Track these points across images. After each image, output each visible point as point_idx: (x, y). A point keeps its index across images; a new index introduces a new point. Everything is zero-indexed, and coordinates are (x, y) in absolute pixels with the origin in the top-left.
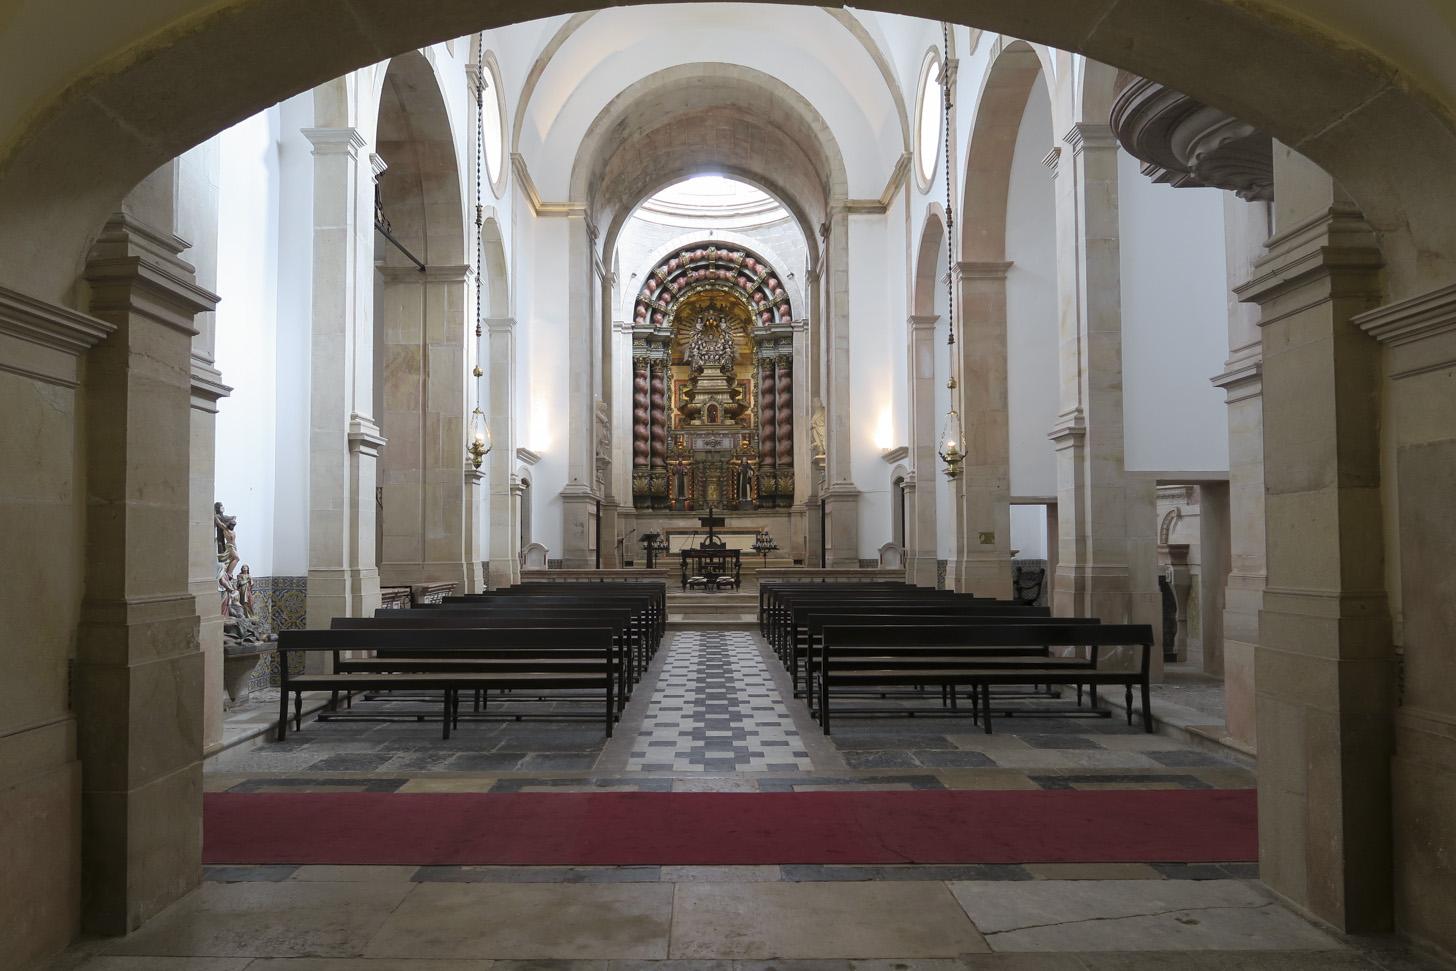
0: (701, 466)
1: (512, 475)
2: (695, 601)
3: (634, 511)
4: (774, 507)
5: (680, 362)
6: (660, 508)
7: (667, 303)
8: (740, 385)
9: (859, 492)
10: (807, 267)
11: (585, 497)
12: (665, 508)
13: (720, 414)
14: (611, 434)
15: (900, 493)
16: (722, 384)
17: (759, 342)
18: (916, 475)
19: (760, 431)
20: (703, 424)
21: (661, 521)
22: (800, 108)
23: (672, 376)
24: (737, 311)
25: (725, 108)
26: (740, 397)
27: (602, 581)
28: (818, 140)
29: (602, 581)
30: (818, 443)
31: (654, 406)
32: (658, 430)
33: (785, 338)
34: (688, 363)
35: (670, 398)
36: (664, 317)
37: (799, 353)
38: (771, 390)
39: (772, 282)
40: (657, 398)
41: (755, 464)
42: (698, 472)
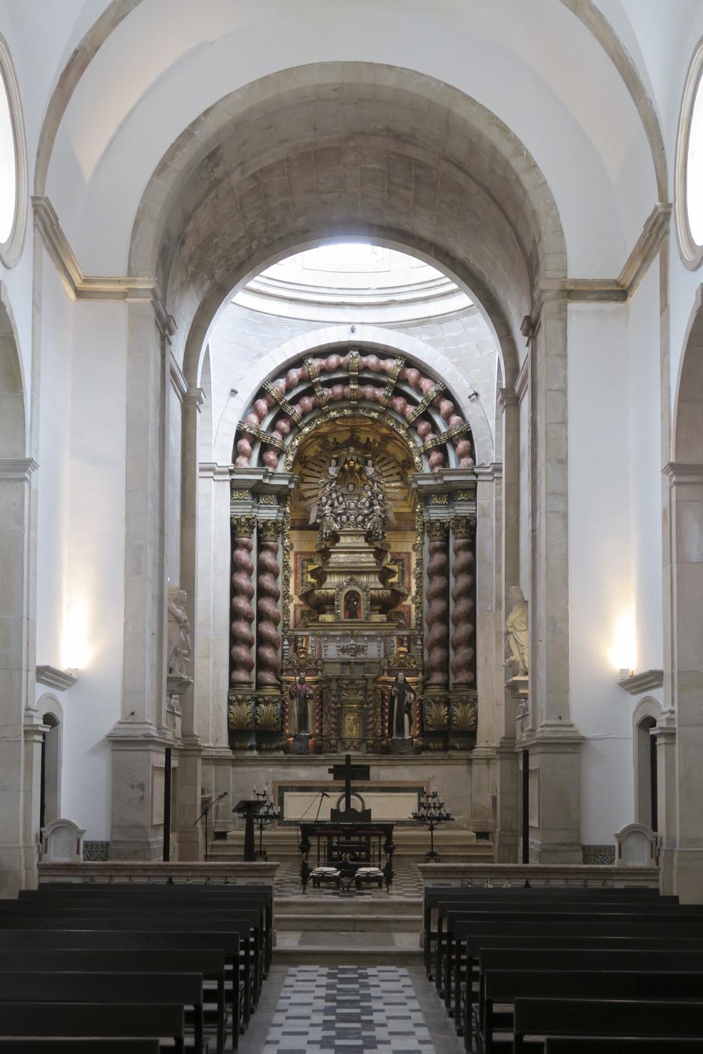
0: (334, 685)
1: (28, 709)
2: (322, 909)
3: (229, 753)
4: (446, 749)
5: (303, 525)
6: (271, 750)
7: (284, 436)
8: (395, 560)
9: (583, 738)
10: (499, 384)
11: (146, 742)
12: (278, 749)
13: (364, 604)
14: (193, 638)
15: (648, 743)
16: (368, 560)
17: (425, 497)
18: (676, 716)
19: (425, 633)
20: (338, 621)
21: (271, 770)
22: (493, 135)
23: (292, 546)
24: (390, 448)
25: (374, 134)
26: (395, 580)
27: (170, 882)
28: (521, 185)
29: (170, 882)
30: (516, 656)
31: (263, 592)
32: (268, 629)
33: (465, 490)
34: (316, 527)
35: (287, 580)
36: (278, 456)
37: (485, 515)
38: (443, 570)
39: (446, 405)
40: (267, 580)
41: (417, 683)
42: (329, 694)
